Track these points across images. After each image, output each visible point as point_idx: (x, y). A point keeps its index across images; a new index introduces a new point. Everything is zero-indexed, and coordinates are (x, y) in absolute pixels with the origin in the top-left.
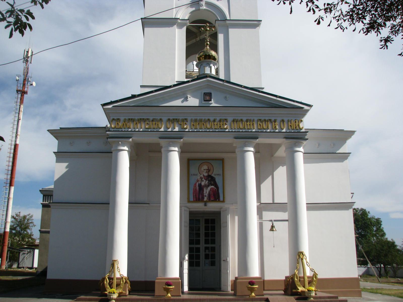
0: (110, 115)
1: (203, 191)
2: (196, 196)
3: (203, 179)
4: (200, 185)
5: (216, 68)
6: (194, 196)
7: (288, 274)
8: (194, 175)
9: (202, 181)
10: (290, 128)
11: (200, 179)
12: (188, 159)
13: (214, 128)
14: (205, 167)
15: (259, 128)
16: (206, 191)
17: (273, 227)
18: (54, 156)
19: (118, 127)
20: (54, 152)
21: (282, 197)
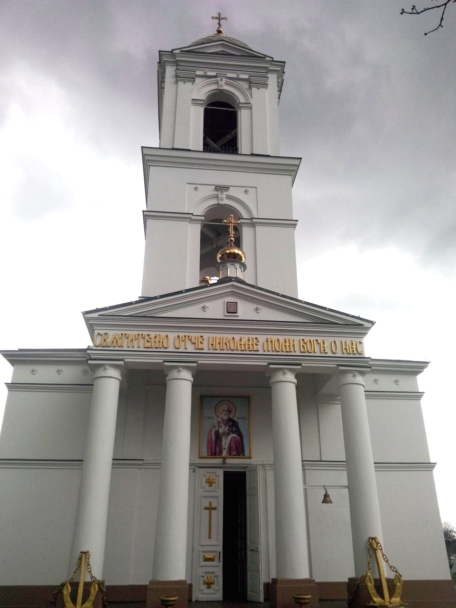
0: (94, 328)
1: (221, 441)
2: (211, 448)
3: (222, 425)
4: (217, 433)
5: (174, 52)
6: (208, 448)
7: (352, 575)
8: (209, 418)
9: (220, 426)
10: (344, 351)
11: (218, 425)
12: (201, 396)
13: (240, 350)
14: (225, 407)
15: (302, 350)
16: (226, 442)
17: (326, 496)
18: (6, 388)
19: (104, 345)
20: (5, 383)
21: (335, 450)
